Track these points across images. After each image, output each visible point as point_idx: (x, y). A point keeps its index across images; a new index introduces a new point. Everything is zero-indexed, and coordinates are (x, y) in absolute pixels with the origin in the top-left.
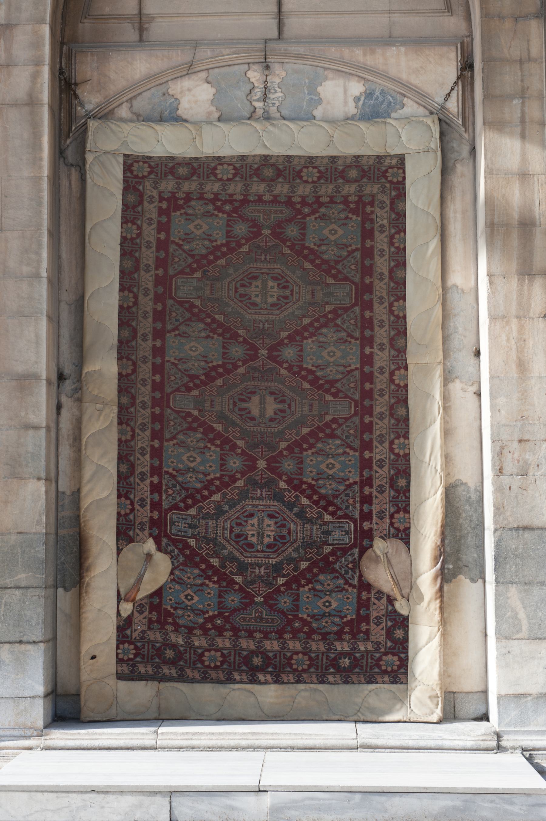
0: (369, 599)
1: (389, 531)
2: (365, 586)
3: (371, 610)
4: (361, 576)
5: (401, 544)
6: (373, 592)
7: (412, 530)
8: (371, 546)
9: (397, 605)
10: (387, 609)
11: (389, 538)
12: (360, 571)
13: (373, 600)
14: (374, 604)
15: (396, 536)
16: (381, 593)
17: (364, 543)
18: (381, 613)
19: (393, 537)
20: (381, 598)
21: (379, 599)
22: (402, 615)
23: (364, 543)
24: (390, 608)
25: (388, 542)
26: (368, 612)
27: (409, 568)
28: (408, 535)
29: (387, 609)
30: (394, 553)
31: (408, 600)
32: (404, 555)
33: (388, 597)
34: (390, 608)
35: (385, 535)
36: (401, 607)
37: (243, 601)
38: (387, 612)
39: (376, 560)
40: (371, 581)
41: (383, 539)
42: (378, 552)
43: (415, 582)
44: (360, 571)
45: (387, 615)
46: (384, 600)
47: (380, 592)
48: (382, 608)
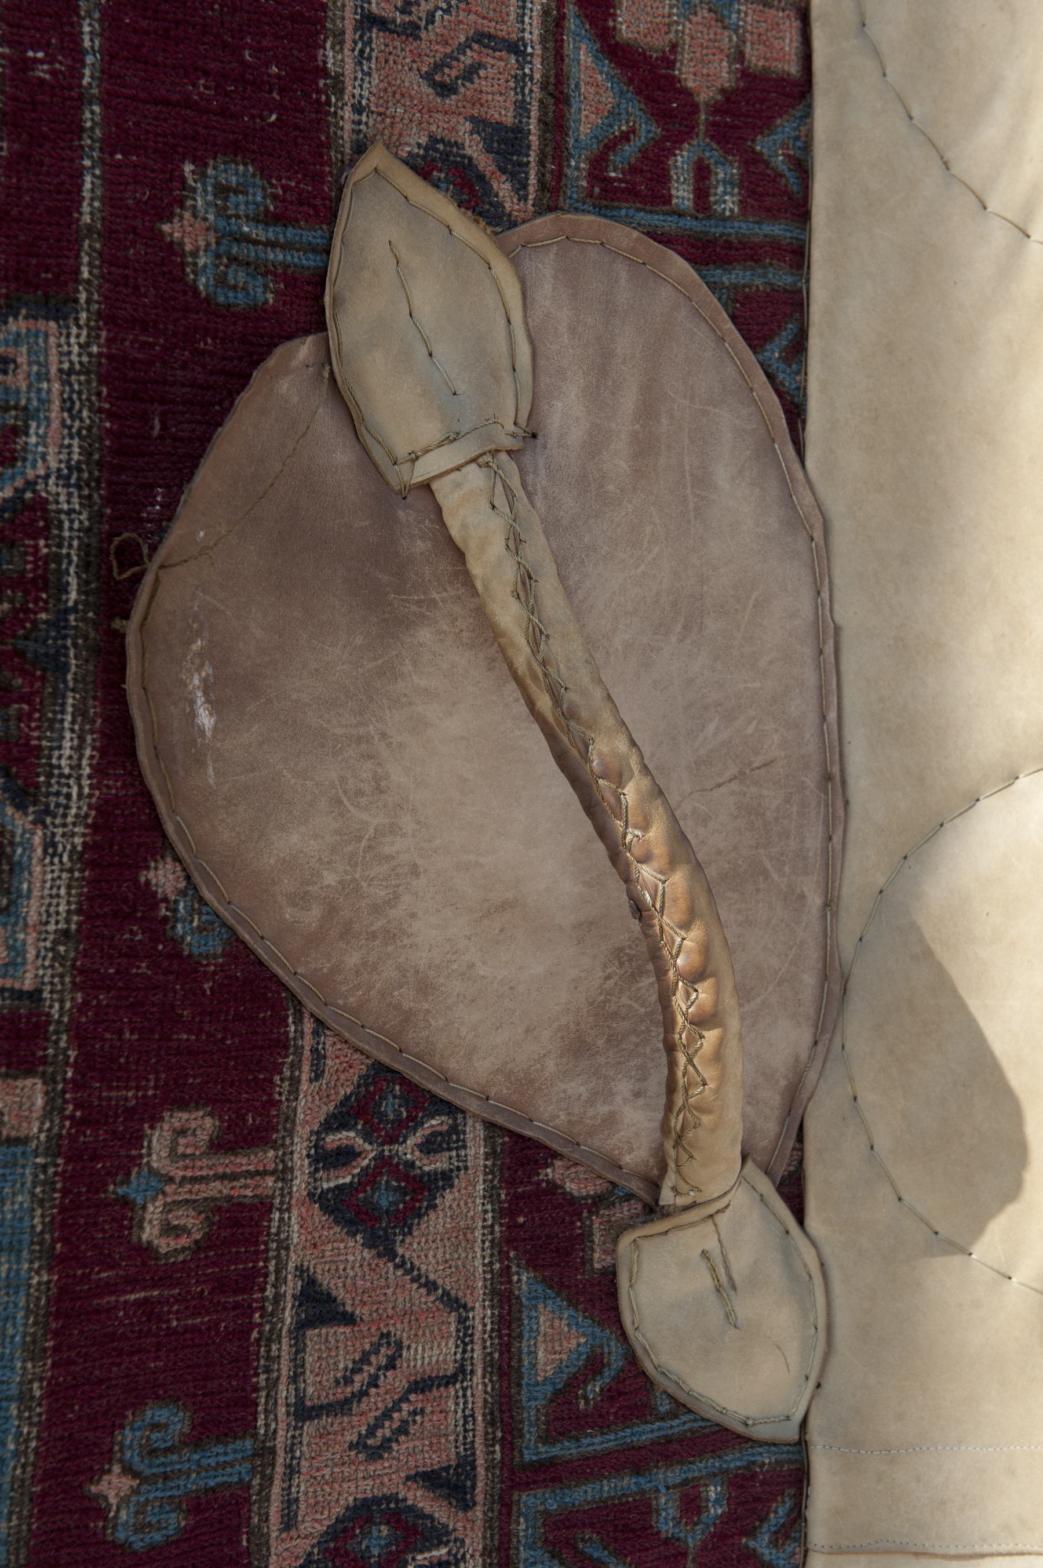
0: (239, 1230)
1: (558, 91)
2: (186, 1009)
3: (276, 1422)
4: (128, 830)
5: (667, 317)
6: (308, 1105)
7: (846, 134)
8: (304, 306)
9: (662, 1283)
10: (506, 1368)
11: (551, 199)
12: (117, 744)
13: (307, 1242)
14: (320, 1307)
15: (629, 188)
16: (422, 1101)
17: (189, 230)
18: (422, 1451)
19: (608, 195)
20: (421, 1191)
21: (380, 1211)
22: (719, 1437)
23: (189, 230)
24: (554, 1341)
25: (545, 268)
26: (222, 1463)
27: (801, 706)
28: (785, 196)
29: (506, 1368)
30: (618, 461)
31: (793, 1192)
32: (738, 498)
33: (521, 1155)
34: (554, 1341)
35: (506, 142)
36: (709, 1314)
37: (136, 569)
38: (504, 1413)
39: (388, 553)
40: (285, 930)
41: (471, 193)
42: (406, 418)
43: (894, 902)
44: (117, 744)
45: (517, 1477)
46: (459, 1233)
47: (394, 1096)
48: (431, 1352)
